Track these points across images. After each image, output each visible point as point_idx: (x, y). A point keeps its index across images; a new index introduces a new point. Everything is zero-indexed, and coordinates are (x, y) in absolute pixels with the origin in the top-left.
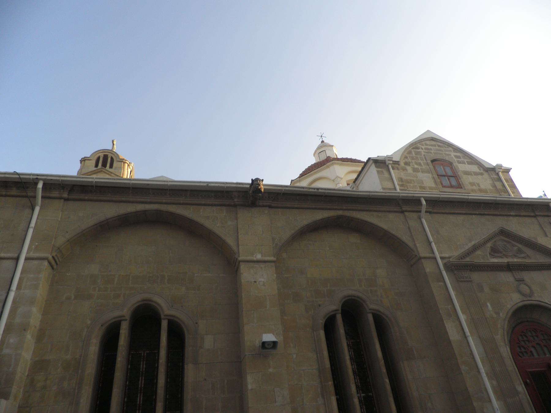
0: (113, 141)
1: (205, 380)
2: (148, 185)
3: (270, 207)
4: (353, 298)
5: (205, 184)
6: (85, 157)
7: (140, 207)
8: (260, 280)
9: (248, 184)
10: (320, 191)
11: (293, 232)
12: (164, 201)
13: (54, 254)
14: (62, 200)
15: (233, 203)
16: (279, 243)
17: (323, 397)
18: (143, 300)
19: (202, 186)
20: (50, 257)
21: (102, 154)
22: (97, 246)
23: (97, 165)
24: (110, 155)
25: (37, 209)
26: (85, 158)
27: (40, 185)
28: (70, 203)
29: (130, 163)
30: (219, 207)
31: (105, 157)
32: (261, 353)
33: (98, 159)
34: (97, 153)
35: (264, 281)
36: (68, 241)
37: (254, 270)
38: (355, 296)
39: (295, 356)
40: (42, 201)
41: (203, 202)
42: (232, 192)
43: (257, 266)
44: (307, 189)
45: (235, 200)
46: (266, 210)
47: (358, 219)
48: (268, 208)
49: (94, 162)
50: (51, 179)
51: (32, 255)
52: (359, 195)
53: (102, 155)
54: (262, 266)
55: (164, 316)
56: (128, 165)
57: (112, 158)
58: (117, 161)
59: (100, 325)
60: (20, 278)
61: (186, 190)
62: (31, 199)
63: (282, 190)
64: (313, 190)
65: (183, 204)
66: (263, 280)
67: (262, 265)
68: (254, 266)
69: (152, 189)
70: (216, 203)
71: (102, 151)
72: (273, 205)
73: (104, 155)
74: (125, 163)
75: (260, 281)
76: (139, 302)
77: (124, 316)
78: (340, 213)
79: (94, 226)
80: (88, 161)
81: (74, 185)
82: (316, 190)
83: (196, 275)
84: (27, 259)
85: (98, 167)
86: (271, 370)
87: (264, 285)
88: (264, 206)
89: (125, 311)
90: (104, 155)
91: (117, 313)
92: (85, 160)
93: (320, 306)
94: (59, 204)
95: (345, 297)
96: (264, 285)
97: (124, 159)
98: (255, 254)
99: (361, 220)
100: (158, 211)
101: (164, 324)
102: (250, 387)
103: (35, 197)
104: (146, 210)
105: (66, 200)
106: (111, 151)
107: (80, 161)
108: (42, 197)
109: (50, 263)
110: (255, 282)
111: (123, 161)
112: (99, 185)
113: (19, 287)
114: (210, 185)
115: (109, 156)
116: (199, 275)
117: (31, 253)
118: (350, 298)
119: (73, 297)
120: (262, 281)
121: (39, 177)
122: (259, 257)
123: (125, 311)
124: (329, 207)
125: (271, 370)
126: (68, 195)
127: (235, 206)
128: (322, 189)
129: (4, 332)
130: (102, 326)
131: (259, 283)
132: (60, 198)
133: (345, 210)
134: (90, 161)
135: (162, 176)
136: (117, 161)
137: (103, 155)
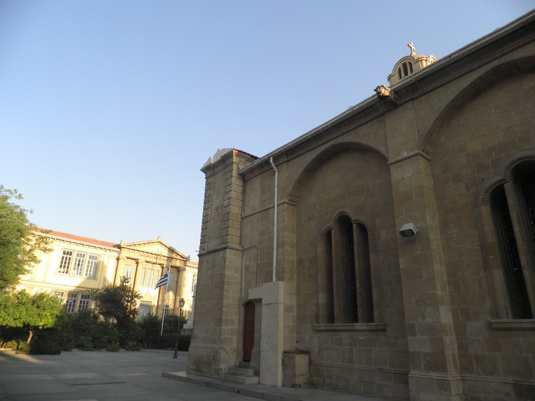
0: (408, 45)
1: (384, 263)
2: (318, 131)
3: (412, 100)
4: (526, 159)
5: (351, 111)
6: (389, 76)
7: (323, 148)
8: (406, 176)
9: (375, 96)
10: (453, 57)
11: (438, 115)
12: (334, 137)
13: (289, 198)
14: (286, 163)
15: (380, 114)
16: (424, 133)
17: (485, 271)
18: (340, 213)
19: (349, 113)
20: (287, 201)
21: (400, 64)
22: (312, 184)
23: (400, 77)
24: (407, 62)
25: (276, 173)
26: (390, 77)
27: (271, 160)
28: (290, 163)
29: (427, 58)
30: (371, 122)
31: (405, 65)
32: (410, 240)
33: (400, 69)
34: (397, 65)
35: (410, 176)
36: (293, 187)
37: (401, 168)
38: (528, 157)
39: (455, 236)
40: (276, 168)
41: (358, 124)
42: (400, 90)
43: (404, 164)
44: (438, 64)
45: (381, 110)
46: (410, 105)
47: (523, 58)
48: (411, 102)
49: (397, 76)
50: (274, 154)
51: (280, 202)
52: (506, 32)
53: (401, 66)
54: (407, 162)
55: (353, 221)
56: (426, 61)
57: (410, 63)
58: (415, 63)
59: (320, 235)
60: (277, 217)
61: (343, 121)
62: (272, 170)
63: (459, 55)
64: (445, 61)
65: (346, 133)
66: (409, 175)
67: (408, 161)
68: (402, 164)
69: (324, 132)
70: (368, 120)
71: (399, 62)
72: (414, 96)
73: (403, 64)
74: (421, 61)
75: (407, 177)
76: (337, 215)
77: (331, 227)
78: (495, 63)
79: (302, 173)
80: (393, 77)
81: (287, 151)
82: (448, 59)
83: (370, 184)
84: (278, 205)
85: (408, 75)
86: (418, 252)
87: (410, 180)
88: (406, 102)
89: (331, 223)
90: (403, 64)
91: (328, 225)
92: (390, 79)
93: (483, 180)
94: (284, 166)
95: (514, 162)
96: (410, 180)
97: (419, 58)
98: (402, 153)
99: (526, 58)
100: (334, 146)
101: (355, 226)
102: (401, 267)
103: (272, 168)
104: (326, 148)
105: (288, 161)
106: (411, 57)
107: (388, 80)
108: (276, 166)
109: (288, 204)
110: (403, 179)
111: (419, 60)
112: (296, 145)
113: (278, 223)
114: (354, 109)
115: (406, 62)
116: (372, 183)
117: (279, 201)
118: (522, 161)
119: (307, 221)
120: (408, 177)
121: (269, 156)
122: (405, 154)
123: (331, 223)
124: (476, 66)
125: (418, 252)
126: (287, 158)
127: (383, 115)
128: (454, 53)
129: (277, 247)
130: (321, 235)
131: (406, 179)
132: (284, 162)
133: (501, 56)
134: (394, 76)
135: (350, 107)
136: (415, 63)
137: (402, 65)
